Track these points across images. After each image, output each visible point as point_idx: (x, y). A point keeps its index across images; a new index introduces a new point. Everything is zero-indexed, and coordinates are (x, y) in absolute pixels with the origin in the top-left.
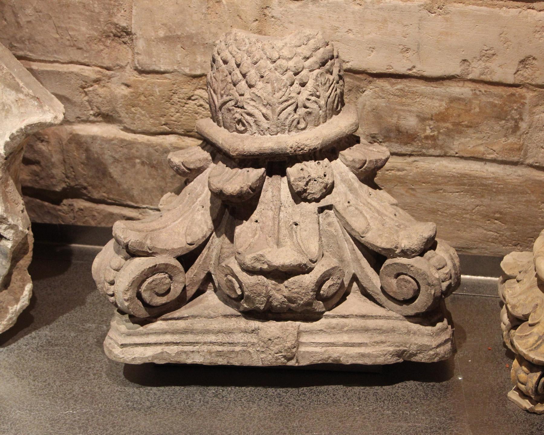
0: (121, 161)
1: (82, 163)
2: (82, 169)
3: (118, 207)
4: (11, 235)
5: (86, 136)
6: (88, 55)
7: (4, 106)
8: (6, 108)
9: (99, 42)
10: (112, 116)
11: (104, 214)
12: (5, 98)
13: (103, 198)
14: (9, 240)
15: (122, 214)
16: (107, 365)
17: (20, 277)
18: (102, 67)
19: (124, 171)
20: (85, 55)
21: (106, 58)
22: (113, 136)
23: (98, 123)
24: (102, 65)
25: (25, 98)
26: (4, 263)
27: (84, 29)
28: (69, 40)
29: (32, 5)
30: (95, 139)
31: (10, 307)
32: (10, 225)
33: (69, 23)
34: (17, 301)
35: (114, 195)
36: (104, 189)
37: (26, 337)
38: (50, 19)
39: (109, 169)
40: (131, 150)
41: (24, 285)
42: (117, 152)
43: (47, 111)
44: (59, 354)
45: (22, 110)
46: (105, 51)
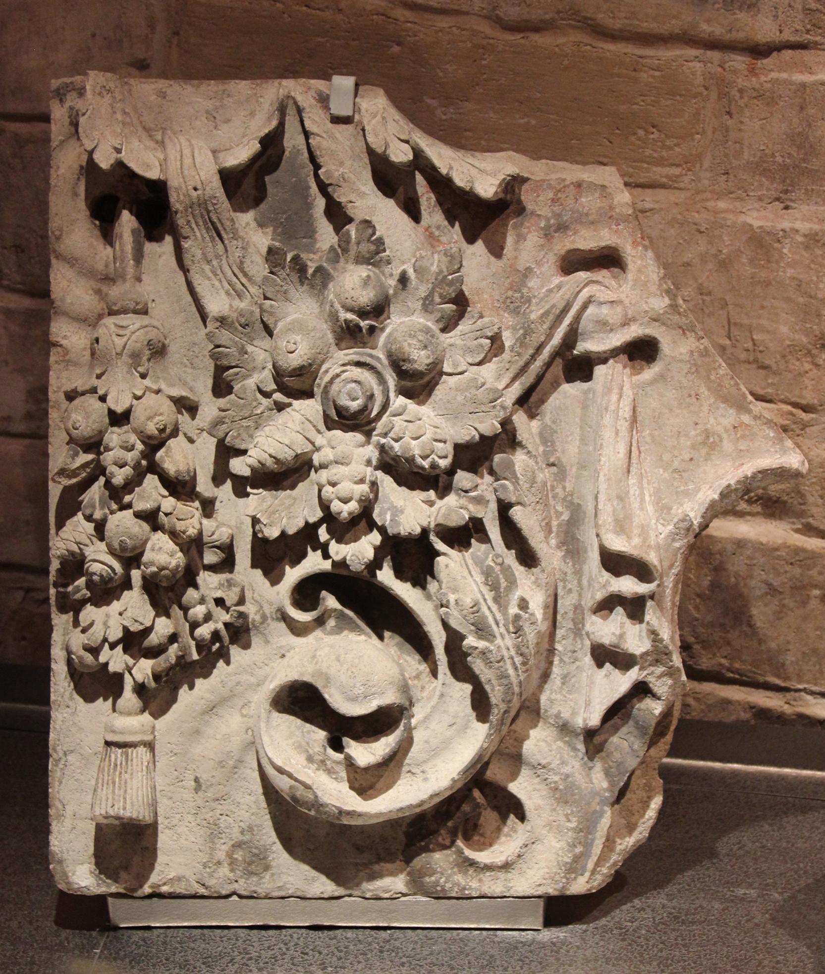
0: (781, 593)
1: (698, 596)
2: (697, 608)
3: (742, 688)
4: (666, 689)
5: (727, 539)
6: (776, 380)
7: (708, 437)
8: (711, 440)
9: (805, 355)
10: (785, 502)
11: (709, 702)
12: (712, 421)
13: (716, 668)
14: (659, 699)
15: (748, 703)
16: (810, 958)
17: (644, 781)
18: (796, 405)
19: (779, 615)
20: (770, 381)
21: (810, 388)
22: (780, 542)
23: (749, 518)
24: (799, 401)
25: (753, 423)
26: (636, 747)
27: (784, 329)
28: (748, 350)
29: (696, 280)
30: (742, 547)
31: (618, 841)
32: (672, 667)
33: (759, 317)
34: (631, 828)
35: (744, 662)
36: (725, 651)
37: (624, 907)
38: (722, 308)
39: (752, 609)
40: (809, 569)
41: (650, 798)
42: (778, 574)
43: (790, 449)
44: (705, 938)
45: (743, 445)
46: (810, 374)
